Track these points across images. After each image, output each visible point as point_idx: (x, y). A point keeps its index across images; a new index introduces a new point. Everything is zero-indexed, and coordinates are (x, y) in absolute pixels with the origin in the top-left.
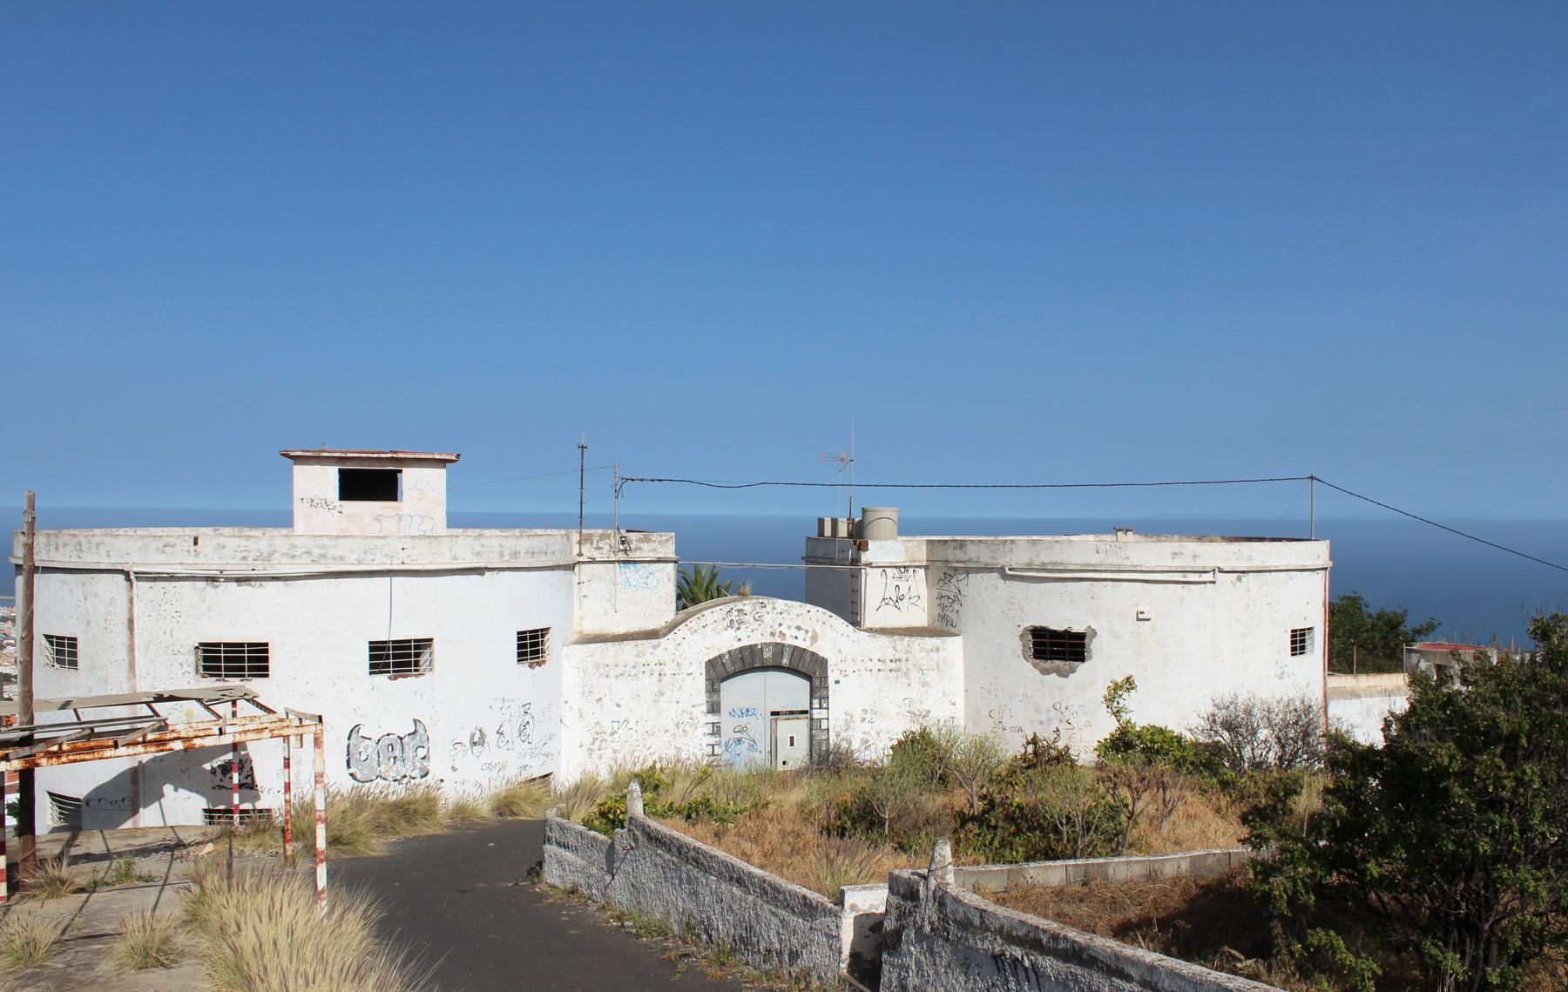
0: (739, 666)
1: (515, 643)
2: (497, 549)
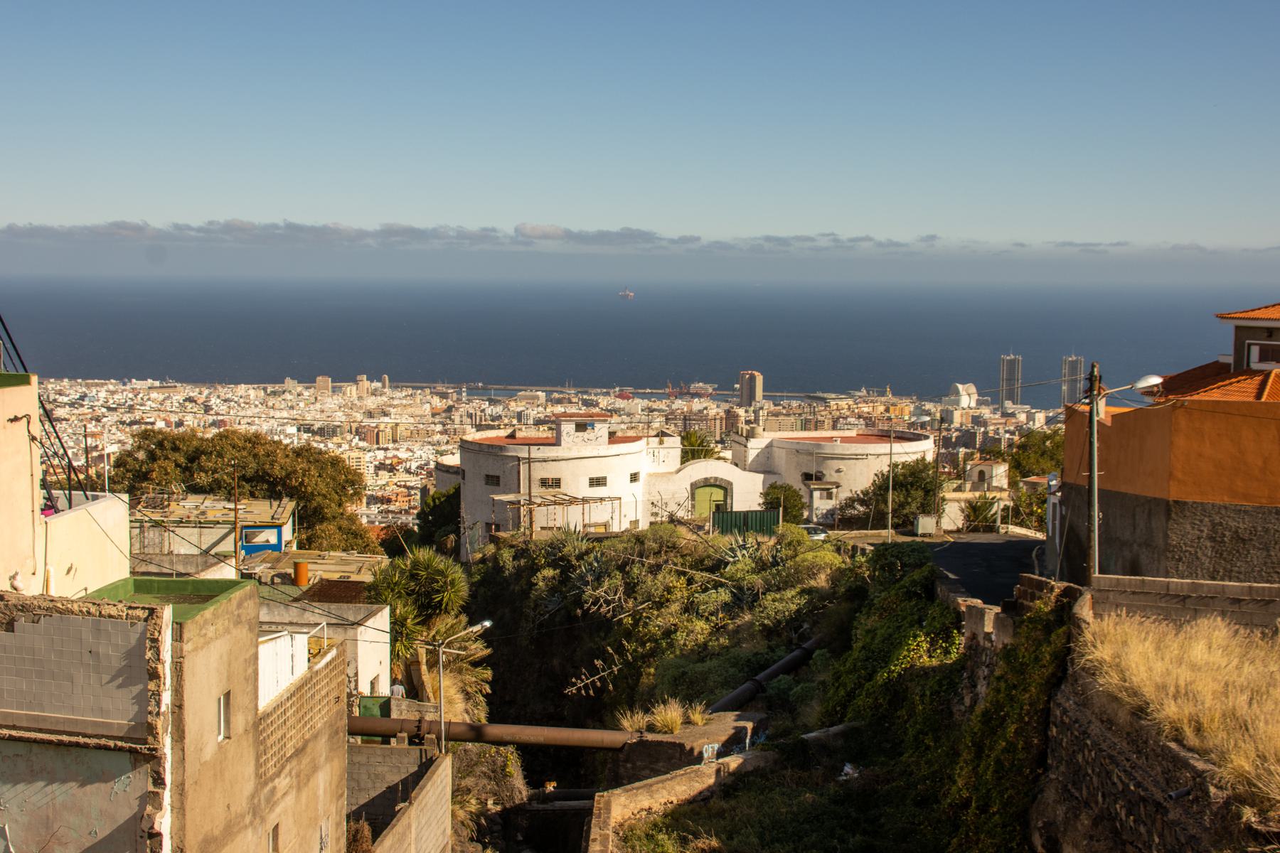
0: (702, 485)
2: (847, 407)
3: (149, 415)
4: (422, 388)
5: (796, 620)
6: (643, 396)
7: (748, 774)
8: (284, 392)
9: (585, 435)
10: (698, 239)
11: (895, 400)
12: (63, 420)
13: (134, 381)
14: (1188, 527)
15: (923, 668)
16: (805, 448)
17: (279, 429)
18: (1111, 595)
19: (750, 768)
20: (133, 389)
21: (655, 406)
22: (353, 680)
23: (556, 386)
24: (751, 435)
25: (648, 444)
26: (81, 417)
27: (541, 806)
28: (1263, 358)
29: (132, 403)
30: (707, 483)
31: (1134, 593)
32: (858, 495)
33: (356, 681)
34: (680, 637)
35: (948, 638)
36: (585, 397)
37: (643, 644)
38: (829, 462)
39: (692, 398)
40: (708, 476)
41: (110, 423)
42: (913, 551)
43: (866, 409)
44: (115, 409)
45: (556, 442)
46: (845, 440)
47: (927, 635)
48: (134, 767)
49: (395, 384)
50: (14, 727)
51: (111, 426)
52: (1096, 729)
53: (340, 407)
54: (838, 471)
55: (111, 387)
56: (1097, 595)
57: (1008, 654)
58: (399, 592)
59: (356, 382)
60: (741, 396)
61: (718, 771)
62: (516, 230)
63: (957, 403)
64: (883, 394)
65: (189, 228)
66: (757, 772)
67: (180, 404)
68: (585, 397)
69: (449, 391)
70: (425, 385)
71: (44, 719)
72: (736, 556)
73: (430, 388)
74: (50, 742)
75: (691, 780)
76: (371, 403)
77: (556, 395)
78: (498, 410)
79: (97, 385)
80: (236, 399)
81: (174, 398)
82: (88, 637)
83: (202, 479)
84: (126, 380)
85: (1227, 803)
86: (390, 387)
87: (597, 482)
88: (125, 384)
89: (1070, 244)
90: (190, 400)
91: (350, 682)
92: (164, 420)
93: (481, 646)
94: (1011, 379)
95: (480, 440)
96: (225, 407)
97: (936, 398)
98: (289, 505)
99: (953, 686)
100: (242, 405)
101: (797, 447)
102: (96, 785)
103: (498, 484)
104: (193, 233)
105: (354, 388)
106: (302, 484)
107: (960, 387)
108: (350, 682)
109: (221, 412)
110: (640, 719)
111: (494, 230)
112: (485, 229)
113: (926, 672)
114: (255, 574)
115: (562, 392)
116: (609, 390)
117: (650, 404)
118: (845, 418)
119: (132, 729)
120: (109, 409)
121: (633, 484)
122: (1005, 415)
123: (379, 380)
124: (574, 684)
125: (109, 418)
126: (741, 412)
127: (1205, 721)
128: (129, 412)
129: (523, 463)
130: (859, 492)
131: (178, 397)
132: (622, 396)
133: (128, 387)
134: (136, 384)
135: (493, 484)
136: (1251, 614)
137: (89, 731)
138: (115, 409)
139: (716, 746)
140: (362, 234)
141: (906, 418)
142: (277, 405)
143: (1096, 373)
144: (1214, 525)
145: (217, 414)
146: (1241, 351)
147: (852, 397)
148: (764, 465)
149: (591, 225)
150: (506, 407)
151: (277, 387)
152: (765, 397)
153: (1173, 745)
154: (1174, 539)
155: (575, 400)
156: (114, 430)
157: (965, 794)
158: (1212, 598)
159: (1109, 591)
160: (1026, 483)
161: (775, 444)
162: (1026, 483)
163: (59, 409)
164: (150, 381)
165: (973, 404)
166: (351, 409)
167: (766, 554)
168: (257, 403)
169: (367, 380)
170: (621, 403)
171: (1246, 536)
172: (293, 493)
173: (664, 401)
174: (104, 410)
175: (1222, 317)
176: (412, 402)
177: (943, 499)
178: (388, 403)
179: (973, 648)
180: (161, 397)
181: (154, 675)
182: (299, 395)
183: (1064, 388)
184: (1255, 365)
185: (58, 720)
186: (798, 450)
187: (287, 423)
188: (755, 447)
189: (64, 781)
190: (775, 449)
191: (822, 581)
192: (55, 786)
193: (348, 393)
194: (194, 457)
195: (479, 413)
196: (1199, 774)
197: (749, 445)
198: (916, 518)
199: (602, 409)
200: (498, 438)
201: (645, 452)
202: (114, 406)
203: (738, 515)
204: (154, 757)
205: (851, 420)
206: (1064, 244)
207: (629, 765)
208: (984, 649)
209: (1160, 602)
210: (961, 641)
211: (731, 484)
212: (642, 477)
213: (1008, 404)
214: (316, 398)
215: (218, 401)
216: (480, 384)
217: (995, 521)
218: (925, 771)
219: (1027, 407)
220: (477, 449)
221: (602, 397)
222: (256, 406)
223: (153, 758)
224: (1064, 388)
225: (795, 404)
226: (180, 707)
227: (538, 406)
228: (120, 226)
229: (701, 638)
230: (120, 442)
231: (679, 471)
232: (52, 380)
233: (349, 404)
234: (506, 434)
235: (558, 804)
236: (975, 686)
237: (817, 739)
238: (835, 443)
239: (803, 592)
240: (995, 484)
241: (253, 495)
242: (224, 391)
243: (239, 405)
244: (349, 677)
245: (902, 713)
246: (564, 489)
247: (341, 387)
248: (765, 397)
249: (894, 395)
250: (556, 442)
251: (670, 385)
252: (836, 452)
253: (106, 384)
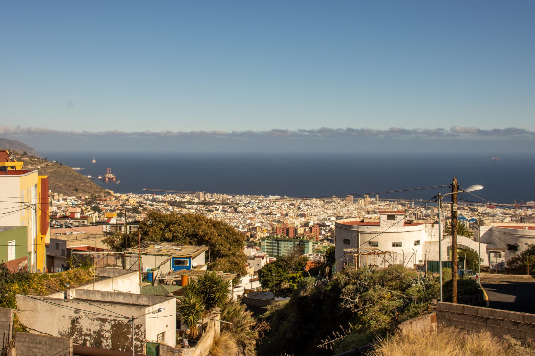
1: (414, 243)
3: (274, 211)
4: (394, 201)
8: (332, 202)
12: (240, 212)
13: (270, 196)
16: (509, 231)
17: (328, 218)
18: (447, 314)
20: (269, 199)
21: (507, 212)
22: (143, 333)
25: (426, 227)
26: (247, 211)
29: (268, 205)
31: (459, 314)
32: (519, 256)
33: (145, 334)
36: (471, 207)
38: (522, 239)
39: (527, 208)
41: (258, 214)
44: (262, 208)
49: (382, 199)
51: (259, 215)
53: (356, 209)
55: (261, 199)
56: (439, 314)
58: (195, 291)
59: (364, 198)
65: (305, 131)
67: (288, 206)
68: (471, 207)
69: (406, 203)
70: (395, 200)
72: (417, 283)
73: (397, 201)
76: (370, 207)
78: (429, 212)
79: (256, 198)
80: (311, 205)
81: (286, 204)
83: (169, 235)
84: (267, 196)
86: (379, 201)
87: (397, 244)
88: (266, 197)
90: (292, 204)
91: (142, 335)
92: (280, 213)
93: (253, 321)
95: (347, 223)
96: (306, 208)
98: (205, 248)
100: (314, 207)
103: (349, 244)
104: (305, 133)
105: (363, 201)
106: (210, 239)
108: (142, 335)
109: (304, 210)
114: (165, 279)
116: (484, 204)
117: (504, 211)
120: (259, 208)
123: (374, 197)
124: (322, 343)
125: (258, 212)
128: (267, 209)
129: (360, 234)
130: (520, 255)
131: (287, 203)
132: (490, 207)
133: (268, 198)
134: (271, 197)
135: (347, 244)
136: (525, 332)
138: (262, 208)
140: (379, 132)
142: (329, 207)
143: (454, 184)
145: (302, 211)
149: (483, 127)
150: (433, 211)
151: (329, 200)
155: (466, 208)
156: (260, 217)
158: (502, 320)
159: (445, 311)
161: (494, 229)
163: (239, 207)
164: (277, 196)
166: (361, 210)
168: (320, 206)
169: (369, 197)
170: (489, 210)
172: (207, 243)
173: (512, 210)
174: (257, 208)
176: (388, 207)
178: (378, 208)
180: (280, 203)
182: (338, 203)
187: (332, 215)
193: (360, 203)
194: (168, 226)
195: (419, 213)
199: (480, 213)
201: (424, 231)
202: (261, 207)
203: (434, 262)
209: (473, 321)
212: (422, 243)
214: (346, 205)
215: (304, 205)
216: (421, 200)
220: (340, 226)
221: (480, 207)
222: (320, 208)
227: (448, 210)
228: (274, 131)
230: (261, 222)
232: (238, 195)
233: (360, 208)
234: (360, 220)
238: (524, 229)
241: (190, 243)
242: (307, 201)
243: (312, 207)
244: (142, 332)
247: (357, 200)
251: (516, 202)
252: (525, 234)
253: (259, 197)
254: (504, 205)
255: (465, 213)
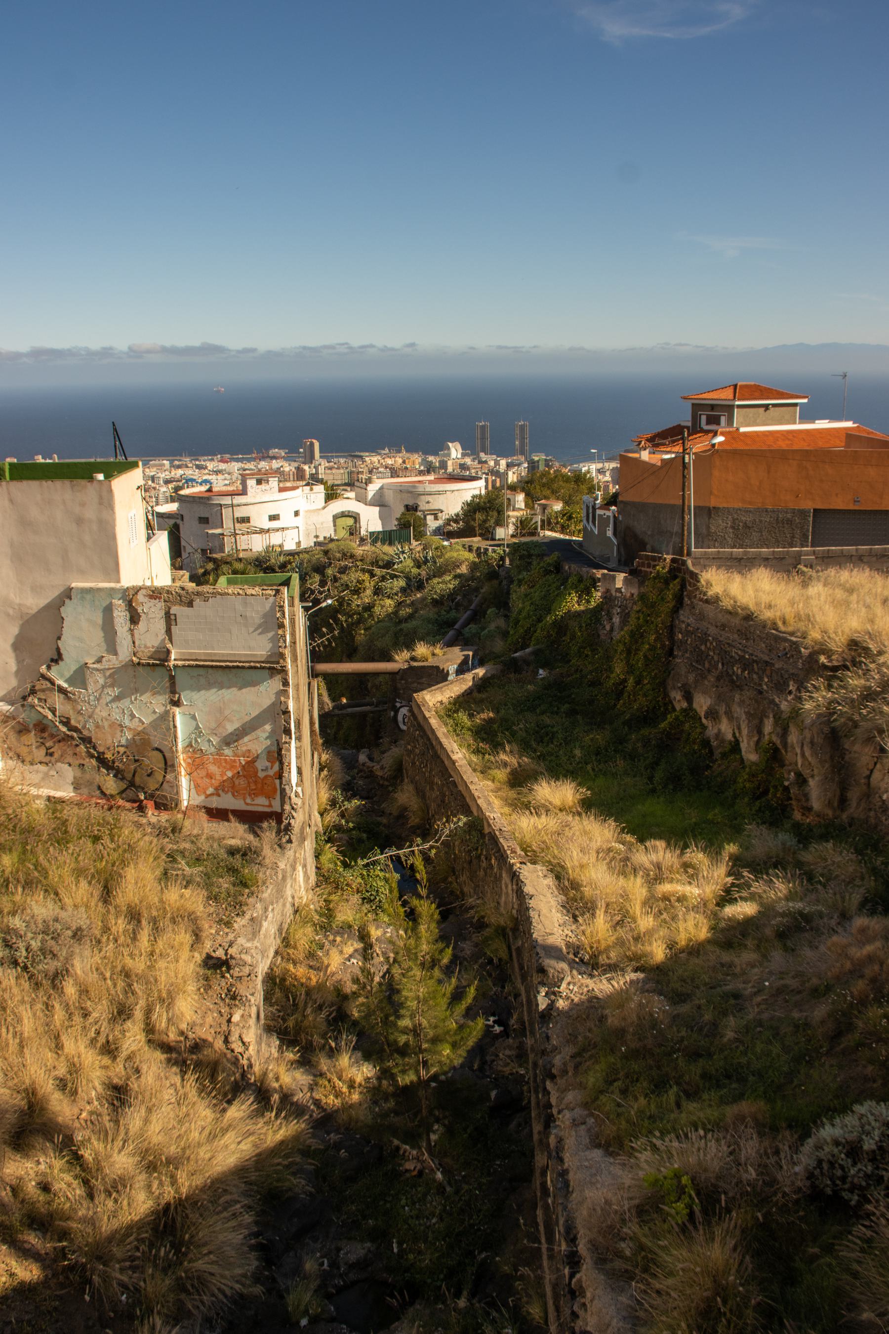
5: (452, 595)
6: (237, 460)
7: (489, 678)
9: (263, 486)
10: (254, 350)
11: (408, 455)
14: (720, 522)
15: (576, 612)
18: (702, 561)
19: (489, 675)
21: (246, 467)
23: (176, 456)
24: (369, 481)
27: (340, 712)
28: (708, 423)
30: (343, 515)
34: (377, 610)
35: (589, 593)
36: (197, 463)
37: (351, 616)
38: (423, 497)
40: (344, 510)
42: (536, 546)
43: (390, 462)
45: (244, 492)
46: (430, 482)
47: (576, 592)
48: (271, 677)
50: (196, 660)
52: (712, 631)
54: (428, 502)
57: (642, 597)
60: (305, 457)
61: (474, 678)
62: (130, 348)
63: (449, 455)
64: (399, 451)
66: (493, 676)
71: (215, 654)
74: (221, 667)
75: (461, 683)
77: (177, 463)
82: (240, 607)
85: (811, 655)
87: (274, 518)
89: (506, 347)
94: (483, 438)
97: (435, 454)
99: (598, 621)
101: (401, 488)
102: (249, 688)
107: (450, 444)
110: (405, 655)
111: (111, 348)
112: (104, 349)
113: (578, 614)
115: (180, 460)
118: (377, 469)
119: (270, 656)
121: (297, 518)
122: (480, 462)
126: (306, 467)
127: (787, 617)
132: (223, 461)
137: (243, 660)
139: (456, 666)
140: (18, 355)
141: (417, 467)
144: (734, 520)
146: (695, 418)
147: (380, 454)
148: (379, 501)
149: (181, 342)
152: (321, 457)
153: (774, 632)
154: (713, 529)
155: (190, 465)
157: (622, 677)
160: (539, 505)
162: (539, 505)
165: (459, 456)
167: (420, 556)
170: (222, 466)
171: (750, 525)
175: (685, 398)
177: (509, 516)
179: (608, 597)
181: (281, 626)
183: (517, 443)
184: (706, 428)
185: (223, 655)
186: (402, 490)
188: (372, 489)
189: (229, 688)
190: (385, 490)
191: (464, 569)
192: (224, 691)
196: (795, 643)
197: (368, 488)
198: (494, 529)
200: (200, 492)
204: (284, 670)
205: (381, 470)
206: (500, 347)
207: (403, 682)
208: (616, 598)
210: (597, 595)
211: (359, 514)
212: (301, 513)
213: (482, 455)
217: (536, 528)
218: (590, 667)
219: (494, 457)
223: (283, 671)
224: (517, 443)
225: (342, 461)
226: (295, 643)
229: (390, 610)
231: (324, 508)
235: (350, 710)
236: (611, 619)
237: (521, 656)
239: (456, 577)
240: (517, 506)
245: (567, 638)
246: (252, 523)
248: (321, 457)
249: (407, 451)
250: (244, 492)
254: (240, 456)
255: (190, 472)
